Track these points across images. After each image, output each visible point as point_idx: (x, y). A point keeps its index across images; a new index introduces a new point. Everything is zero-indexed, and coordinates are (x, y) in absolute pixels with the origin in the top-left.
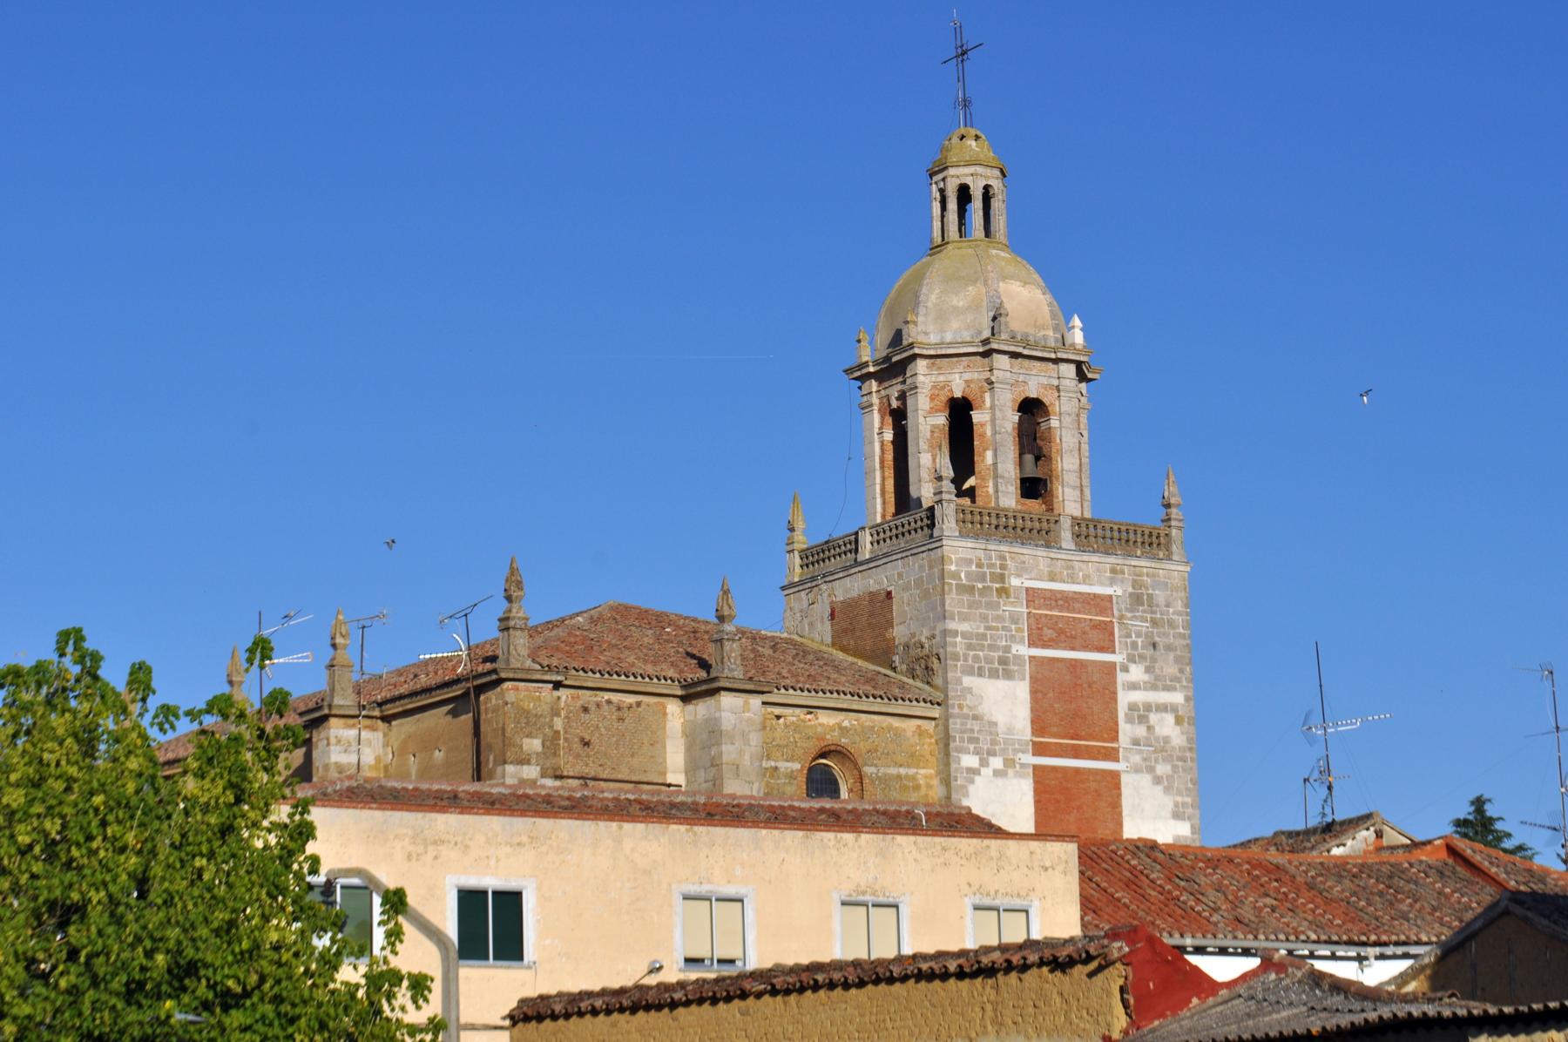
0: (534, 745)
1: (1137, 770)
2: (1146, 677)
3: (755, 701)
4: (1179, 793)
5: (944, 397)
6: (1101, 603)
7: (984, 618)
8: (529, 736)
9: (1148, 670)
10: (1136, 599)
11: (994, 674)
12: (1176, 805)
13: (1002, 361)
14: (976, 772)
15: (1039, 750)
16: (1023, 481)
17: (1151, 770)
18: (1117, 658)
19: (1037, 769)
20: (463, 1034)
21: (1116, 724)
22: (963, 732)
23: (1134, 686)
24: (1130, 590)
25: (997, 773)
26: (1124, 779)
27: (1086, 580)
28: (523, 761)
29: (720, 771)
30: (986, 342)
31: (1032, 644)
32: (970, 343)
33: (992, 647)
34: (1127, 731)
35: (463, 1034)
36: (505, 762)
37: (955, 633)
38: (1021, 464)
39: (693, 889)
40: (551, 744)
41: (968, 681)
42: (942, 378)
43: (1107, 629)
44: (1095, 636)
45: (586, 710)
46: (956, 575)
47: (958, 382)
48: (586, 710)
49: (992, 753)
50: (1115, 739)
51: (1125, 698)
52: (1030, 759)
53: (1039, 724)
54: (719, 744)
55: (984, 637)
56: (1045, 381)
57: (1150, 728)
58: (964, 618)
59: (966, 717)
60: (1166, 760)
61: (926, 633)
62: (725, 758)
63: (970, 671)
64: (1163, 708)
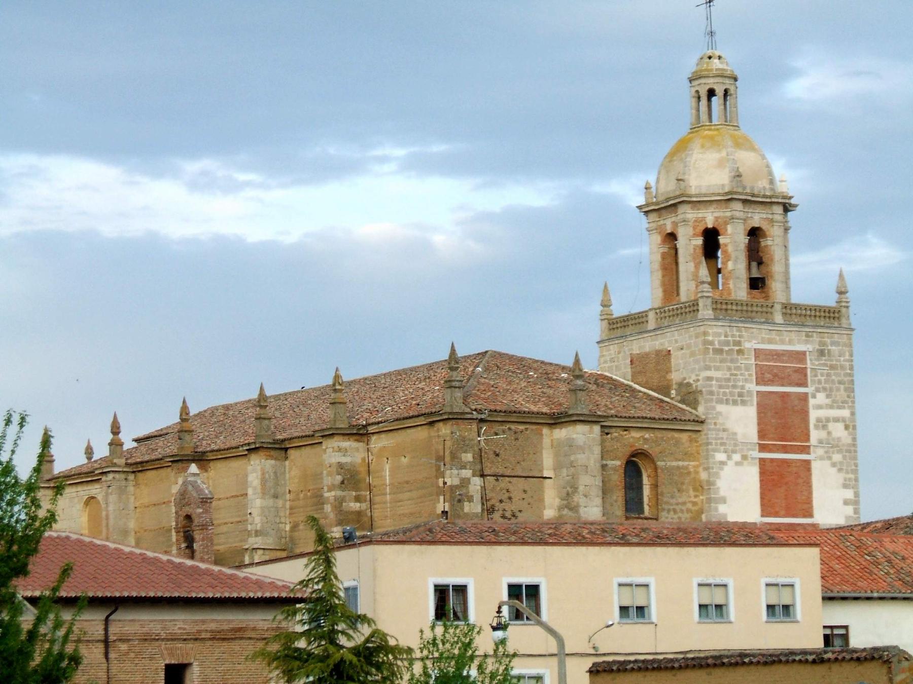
1: (821, 458)
2: (828, 401)
3: (597, 429)
4: (847, 472)
5: (701, 228)
6: (800, 356)
7: (729, 369)
9: (828, 396)
10: (821, 353)
11: (735, 403)
12: (845, 480)
14: (723, 463)
15: (763, 448)
17: (830, 458)
19: (762, 461)
23: (819, 407)
24: (817, 347)
25: (737, 464)
27: (791, 342)
31: (757, 384)
32: (719, 194)
33: (734, 387)
41: (720, 408)
42: (700, 215)
43: (803, 372)
44: (795, 377)
49: (734, 452)
50: (808, 440)
51: (814, 415)
53: (762, 434)
57: (829, 433)
59: (719, 430)
61: (694, 377)
63: (720, 401)
64: (837, 420)
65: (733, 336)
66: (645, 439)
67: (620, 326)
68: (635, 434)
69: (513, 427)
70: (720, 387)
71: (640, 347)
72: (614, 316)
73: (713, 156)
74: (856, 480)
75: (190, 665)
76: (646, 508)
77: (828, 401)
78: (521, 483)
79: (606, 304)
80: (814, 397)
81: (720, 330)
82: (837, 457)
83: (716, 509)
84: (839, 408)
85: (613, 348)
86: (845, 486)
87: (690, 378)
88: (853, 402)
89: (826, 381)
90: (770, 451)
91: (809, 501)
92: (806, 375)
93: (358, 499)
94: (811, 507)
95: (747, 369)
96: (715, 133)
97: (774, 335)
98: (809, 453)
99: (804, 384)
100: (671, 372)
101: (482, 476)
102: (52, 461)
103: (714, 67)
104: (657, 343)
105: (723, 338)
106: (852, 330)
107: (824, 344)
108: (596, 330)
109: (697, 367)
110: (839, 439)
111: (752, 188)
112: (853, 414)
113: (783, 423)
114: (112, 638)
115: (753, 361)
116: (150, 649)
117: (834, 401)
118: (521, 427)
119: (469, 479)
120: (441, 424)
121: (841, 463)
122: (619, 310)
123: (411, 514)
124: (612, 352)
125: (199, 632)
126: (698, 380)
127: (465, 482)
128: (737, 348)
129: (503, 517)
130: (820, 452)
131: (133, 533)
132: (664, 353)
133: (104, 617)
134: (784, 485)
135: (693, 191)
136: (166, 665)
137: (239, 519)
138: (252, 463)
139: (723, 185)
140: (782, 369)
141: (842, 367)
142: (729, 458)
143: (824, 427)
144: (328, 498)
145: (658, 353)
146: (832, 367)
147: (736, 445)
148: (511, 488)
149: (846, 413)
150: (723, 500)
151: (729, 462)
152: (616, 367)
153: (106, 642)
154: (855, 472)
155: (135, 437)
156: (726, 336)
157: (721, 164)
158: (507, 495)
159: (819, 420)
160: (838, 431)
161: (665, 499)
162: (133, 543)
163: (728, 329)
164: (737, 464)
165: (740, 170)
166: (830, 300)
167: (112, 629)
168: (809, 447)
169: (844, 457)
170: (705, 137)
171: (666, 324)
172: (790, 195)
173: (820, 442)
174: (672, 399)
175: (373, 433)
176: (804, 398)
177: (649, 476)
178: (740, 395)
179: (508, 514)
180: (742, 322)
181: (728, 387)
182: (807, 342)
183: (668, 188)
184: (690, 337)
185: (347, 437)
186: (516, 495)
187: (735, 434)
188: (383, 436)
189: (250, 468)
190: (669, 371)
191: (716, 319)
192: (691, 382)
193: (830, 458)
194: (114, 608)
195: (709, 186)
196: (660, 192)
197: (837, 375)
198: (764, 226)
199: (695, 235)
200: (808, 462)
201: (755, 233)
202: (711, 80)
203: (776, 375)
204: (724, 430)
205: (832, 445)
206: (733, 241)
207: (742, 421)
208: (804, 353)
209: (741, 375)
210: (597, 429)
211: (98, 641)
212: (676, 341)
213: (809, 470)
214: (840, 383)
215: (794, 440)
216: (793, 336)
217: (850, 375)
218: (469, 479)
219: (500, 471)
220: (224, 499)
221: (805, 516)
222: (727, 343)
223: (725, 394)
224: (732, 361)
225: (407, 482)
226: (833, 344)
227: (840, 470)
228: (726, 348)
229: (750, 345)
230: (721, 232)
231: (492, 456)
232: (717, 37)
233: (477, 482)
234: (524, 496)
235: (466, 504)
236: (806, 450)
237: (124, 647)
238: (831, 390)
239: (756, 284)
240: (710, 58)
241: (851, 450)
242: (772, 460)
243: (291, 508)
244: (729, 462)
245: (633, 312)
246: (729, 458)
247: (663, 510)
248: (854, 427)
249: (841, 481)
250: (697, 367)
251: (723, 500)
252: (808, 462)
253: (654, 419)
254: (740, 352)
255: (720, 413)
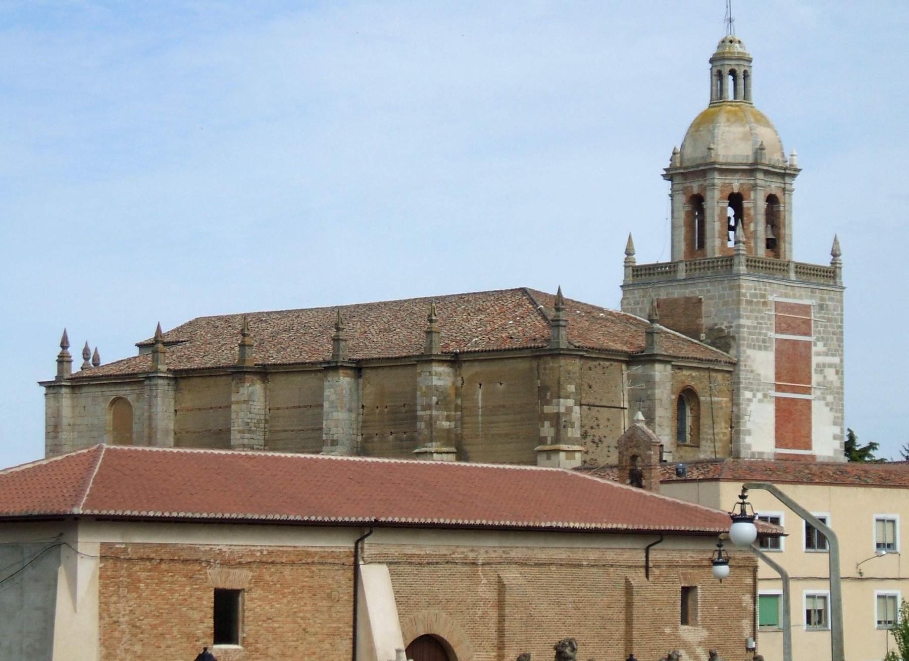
0: (572, 388)
1: (819, 399)
2: (825, 349)
3: (669, 367)
4: (836, 412)
5: (728, 193)
6: (806, 309)
7: (756, 318)
8: (570, 383)
9: (825, 345)
10: (821, 307)
11: (760, 348)
12: (835, 417)
13: (760, 176)
14: (750, 400)
15: (779, 388)
16: (768, 240)
17: (824, 399)
18: (812, 339)
19: (778, 399)
20: (828, 576)
21: (810, 373)
22: (746, 379)
23: (818, 354)
24: (819, 302)
25: (760, 401)
26: (813, 403)
27: (800, 297)
28: (567, 397)
29: (654, 404)
30: (751, 164)
31: (776, 332)
32: (745, 164)
33: (760, 334)
34: (815, 378)
35: (828, 576)
36: (559, 398)
37: (743, 326)
38: (766, 231)
39: (881, 516)
40: (579, 388)
41: (749, 352)
42: (727, 181)
43: (807, 323)
44: (803, 327)
45: (590, 369)
46: (745, 295)
47: (736, 184)
48: (590, 369)
49: (758, 391)
50: (810, 383)
51: (815, 360)
52: (773, 393)
53: (778, 377)
54: (653, 388)
55: (755, 328)
56: (778, 185)
57: (825, 377)
58: (748, 318)
59: (747, 371)
60: (831, 393)
61: (726, 324)
62: (657, 396)
63: (749, 346)
64: (830, 366)
65: (760, 289)
66: (693, 377)
67: (640, 276)
68: (686, 373)
69: (602, 363)
70: (750, 334)
71: (668, 294)
72: (637, 264)
73: (738, 130)
74: (842, 418)
75: (696, 587)
76: (688, 437)
77: (825, 349)
78: (605, 413)
79: (629, 252)
80: (815, 345)
81: (751, 284)
82: (830, 398)
83: (744, 440)
84: (833, 355)
85: (638, 294)
86: (835, 424)
87: (722, 324)
88: (842, 351)
89: (824, 332)
90: (783, 391)
91: (809, 435)
92: (810, 326)
93: (448, 418)
94: (810, 441)
95: (769, 319)
96: (737, 108)
97: (789, 290)
98: (810, 394)
99: (808, 334)
100: (701, 317)
101: (581, 405)
102: (70, 362)
103: (736, 50)
104: (687, 291)
105: (753, 291)
106: (844, 288)
107: (822, 299)
108: (619, 275)
109: (730, 315)
110: (832, 382)
111: (770, 160)
112: (842, 361)
113: (793, 367)
114: (651, 564)
115: (773, 313)
116: (673, 574)
117: (829, 350)
118: (607, 363)
119: (571, 408)
120: (549, 358)
121: (832, 403)
122: (641, 259)
123: (507, 435)
124: (637, 296)
125: (702, 560)
126: (731, 327)
127: (569, 410)
128: (762, 300)
129: (593, 442)
130: (818, 393)
131: (173, 433)
132: (694, 301)
133: (645, 546)
134: (792, 421)
135: (721, 160)
136: (683, 588)
137: (300, 428)
138: (330, 379)
139: (748, 156)
140: (793, 321)
141: (836, 321)
142: (754, 396)
143: (822, 372)
144: (422, 416)
145: (687, 300)
146: (829, 320)
147: (759, 385)
148: (599, 417)
149: (836, 360)
150: (749, 433)
151: (754, 400)
152: (640, 309)
153: (647, 568)
154: (842, 411)
155: (138, 342)
156: (755, 290)
157: (745, 138)
158: (596, 422)
159: (818, 365)
160: (831, 374)
161: (705, 430)
162: (172, 443)
163: (756, 283)
164: (760, 401)
165: (764, 144)
166: (825, 261)
167: (651, 557)
168: (810, 388)
169: (835, 398)
170: (729, 112)
171: (697, 275)
172: (799, 167)
173: (818, 384)
174: (701, 341)
175: (464, 361)
176: (808, 345)
177: (691, 409)
178: (764, 341)
179: (596, 440)
180: (768, 278)
181: (754, 334)
182: (811, 297)
183: (694, 154)
184: (724, 289)
185: (441, 364)
186: (603, 423)
187: (759, 375)
188: (476, 364)
189: (326, 384)
190: (699, 316)
191: (749, 275)
192: (723, 327)
193: (824, 399)
194: (658, 539)
195: (735, 156)
196: (686, 157)
197: (832, 327)
198: (779, 194)
199: (721, 198)
200: (809, 401)
201: (772, 200)
202: (733, 62)
203: (789, 325)
204: (752, 372)
205: (827, 388)
206: (756, 204)
207: (760, 363)
208: (809, 307)
209: (765, 324)
210: (669, 367)
211: (641, 567)
212: (709, 291)
213: (810, 408)
214: (834, 333)
215: (800, 382)
216: (802, 291)
217: (841, 327)
218: (571, 408)
219: (592, 401)
220: (283, 408)
221: (806, 449)
222: (755, 296)
223: (753, 340)
224: (759, 311)
225: (503, 406)
226: (831, 299)
227: (831, 409)
228: (755, 300)
229: (772, 298)
230: (745, 197)
231: (586, 387)
232: (734, 23)
233: (577, 409)
234: (608, 423)
235: (569, 429)
236: (807, 391)
237: (657, 571)
238: (827, 340)
239: (772, 244)
240: (731, 42)
241: (839, 392)
242: (785, 399)
243: (364, 422)
244: (754, 400)
245: (660, 262)
246: (754, 396)
247: (703, 439)
248: (842, 374)
249: (832, 419)
250: (730, 315)
251: (749, 433)
252: (809, 401)
253: (711, 361)
254: (765, 303)
255: (748, 357)
